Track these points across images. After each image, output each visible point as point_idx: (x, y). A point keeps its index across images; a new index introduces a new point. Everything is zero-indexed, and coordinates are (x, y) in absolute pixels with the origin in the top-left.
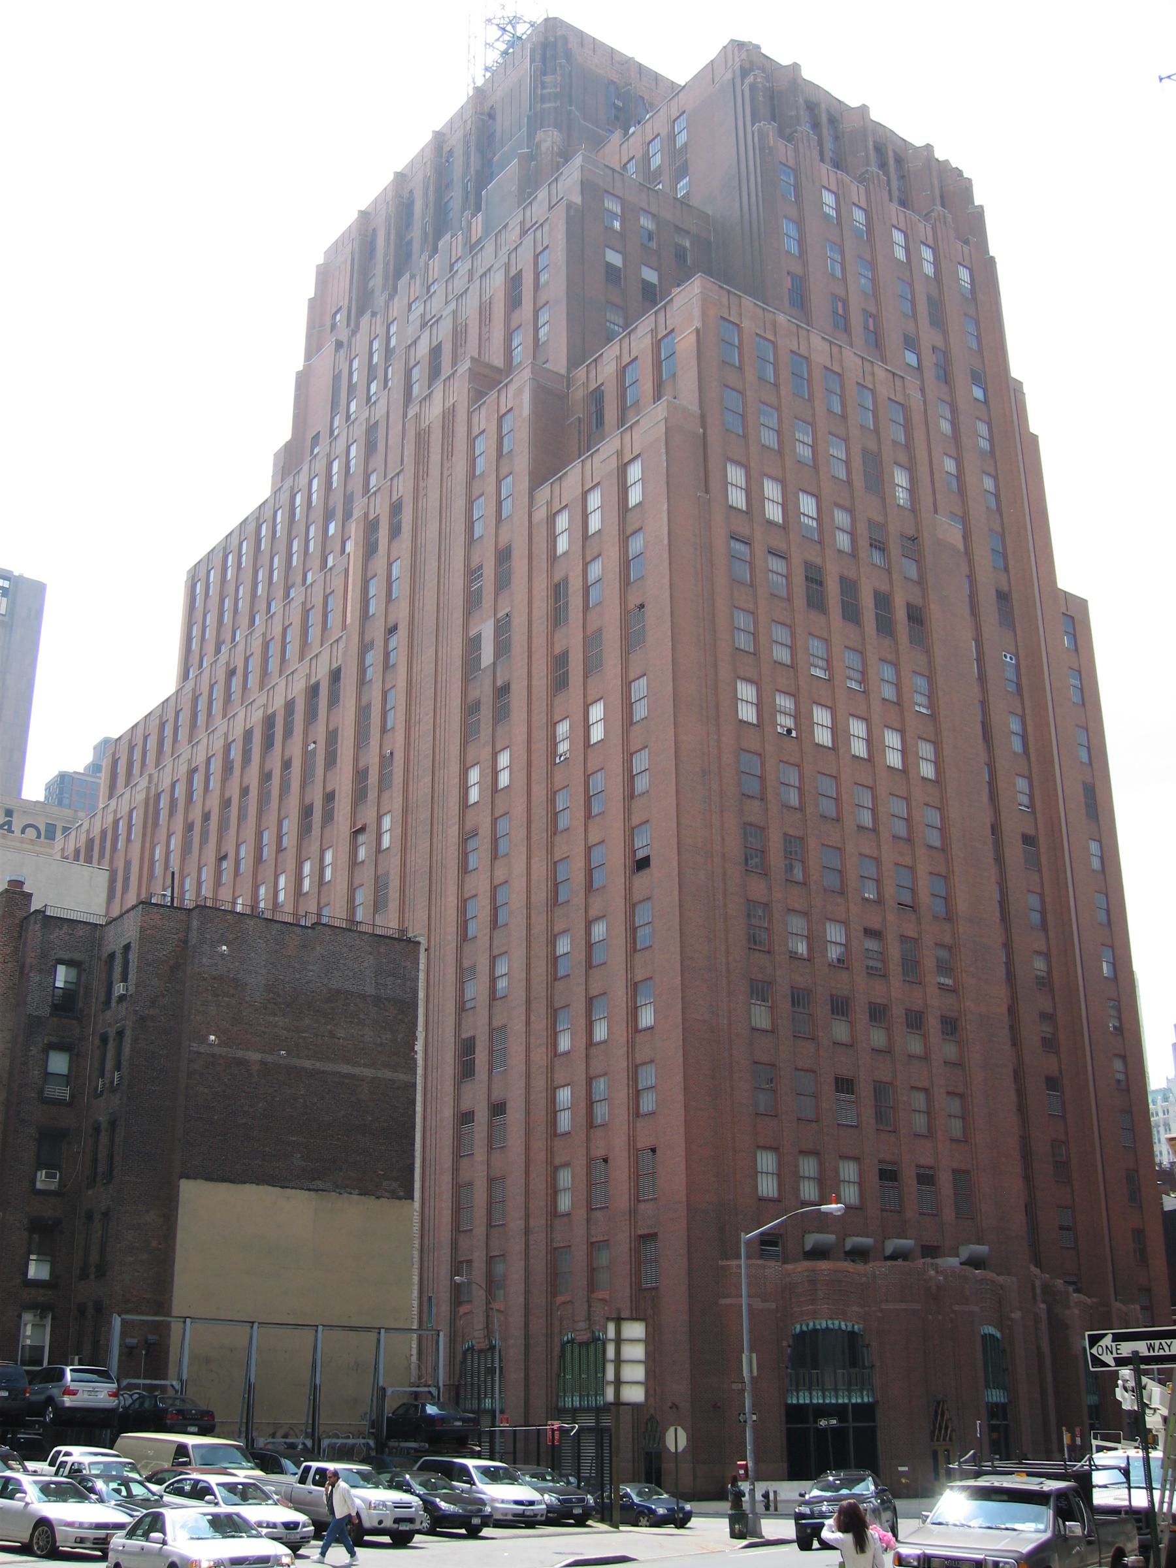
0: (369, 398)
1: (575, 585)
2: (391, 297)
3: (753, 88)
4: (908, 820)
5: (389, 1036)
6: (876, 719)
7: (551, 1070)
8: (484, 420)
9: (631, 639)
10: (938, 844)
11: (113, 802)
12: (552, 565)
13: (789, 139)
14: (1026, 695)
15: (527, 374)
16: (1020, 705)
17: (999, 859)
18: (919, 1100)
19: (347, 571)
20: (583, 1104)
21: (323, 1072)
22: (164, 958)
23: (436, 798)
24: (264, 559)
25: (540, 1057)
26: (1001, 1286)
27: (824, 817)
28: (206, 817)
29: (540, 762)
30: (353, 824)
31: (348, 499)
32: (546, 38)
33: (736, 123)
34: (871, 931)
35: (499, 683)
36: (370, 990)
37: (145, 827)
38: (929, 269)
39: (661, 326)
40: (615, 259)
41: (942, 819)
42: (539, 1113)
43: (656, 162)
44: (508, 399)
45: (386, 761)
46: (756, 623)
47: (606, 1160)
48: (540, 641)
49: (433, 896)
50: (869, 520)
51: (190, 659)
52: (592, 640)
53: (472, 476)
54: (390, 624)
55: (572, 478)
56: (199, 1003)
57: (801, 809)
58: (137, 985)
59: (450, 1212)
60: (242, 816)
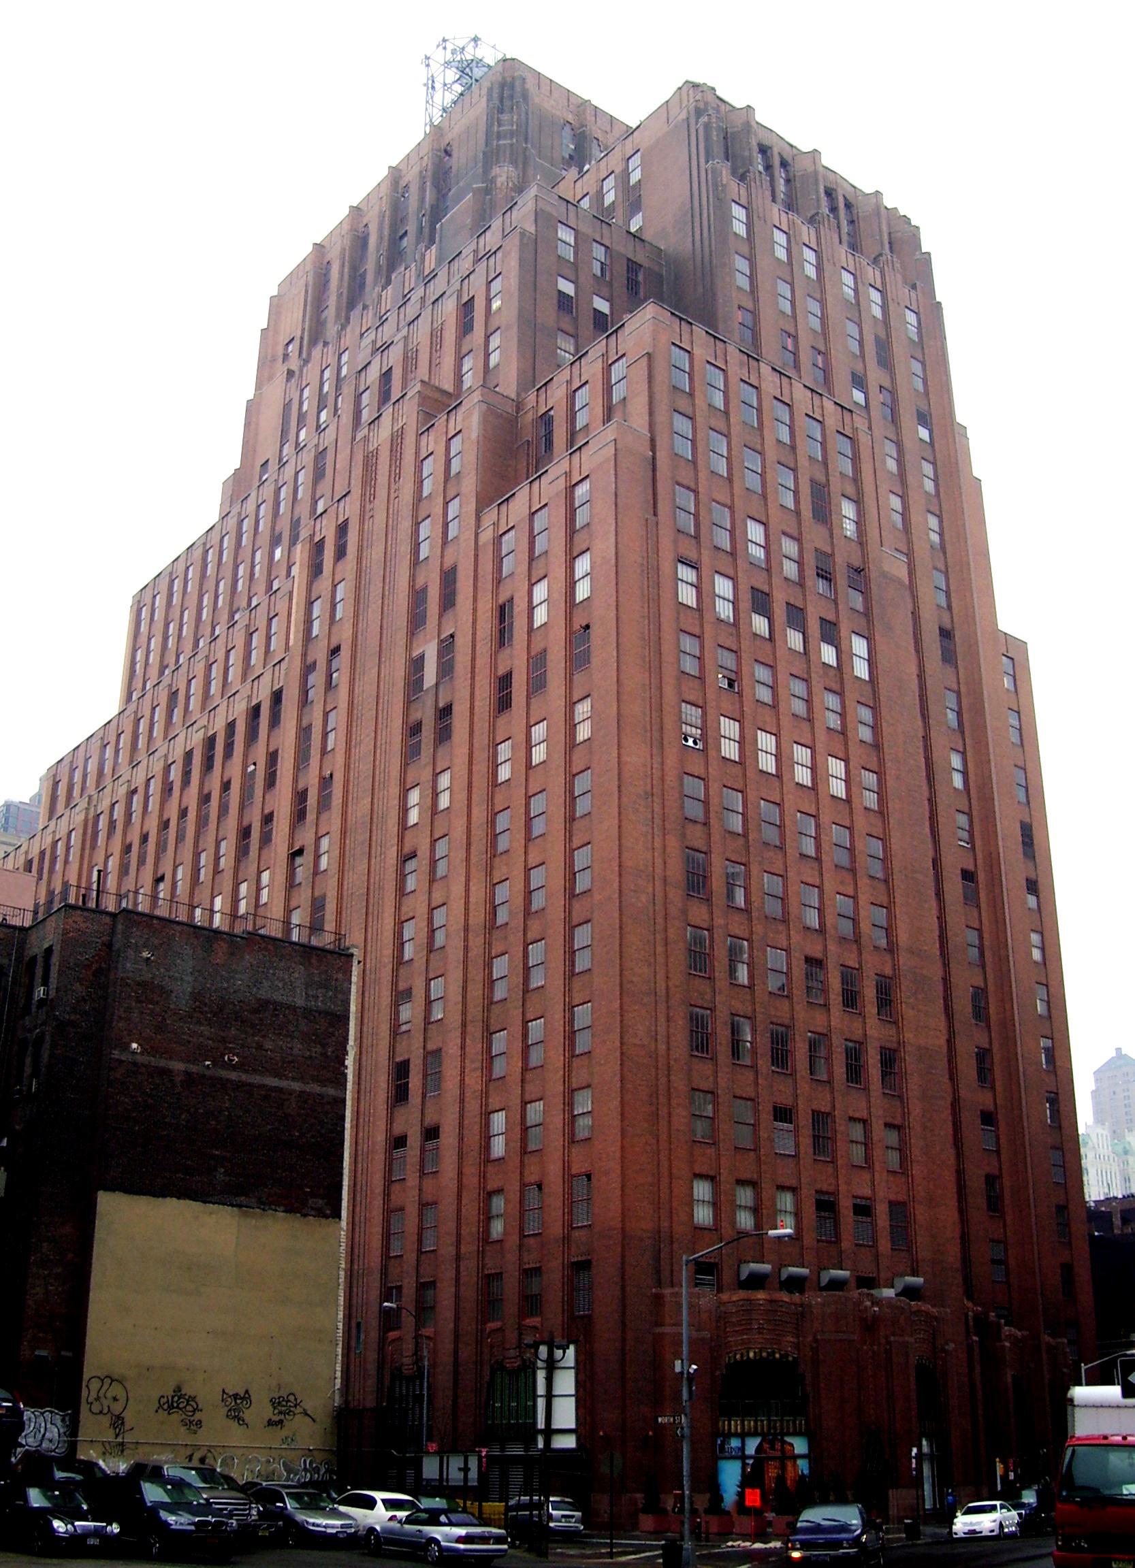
0: (318, 426)
1: (520, 606)
2: (343, 327)
3: (707, 126)
4: (851, 850)
5: (319, 1049)
6: (820, 747)
7: (485, 1094)
8: (432, 442)
9: (577, 659)
10: (880, 875)
11: (53, 823)
12: (498, 587)
13: (742, 178)
14: (967, 733)
15: (476, 396)
16: (961, 742)
17: (939, 894)
18: (857, 1132)
19: (291, 593)
20: (518, 1129)
21: (250, 1084)
22: (86, 962)
23: (375, 820)
24: (210, 585)
25: (474, 1081)
26: (936, 1318)
27: (766, 844)
28: (145, 838)
29: (480, 782)
30: (291, 845)
31: (295, 525)
32: (504, 78)
33: (689, 151)
34: (812, 959)
35: (441, 705)
36: (300, 1002)
37: (83, 849)
38: (877, 312)
39: (612, 352)
40: (567, 288)
41: (884, 850)
42: (473, 1137)
43: (609, 198)
44: (458, 420)
45: (326, 782)
46: (702, 647)
47: (540, 1187)
48: (483, 661)
49: (370, 919)
50: (816, 550)
51: (134, 683)
52: (538, 661)
53: (418, 498)
54: (333, 645)
55: (518, 507)
56: (122, 1009)
57: (745, 835)
58: (58, 990)
59: (380, 1237)
60: (180, 838)
